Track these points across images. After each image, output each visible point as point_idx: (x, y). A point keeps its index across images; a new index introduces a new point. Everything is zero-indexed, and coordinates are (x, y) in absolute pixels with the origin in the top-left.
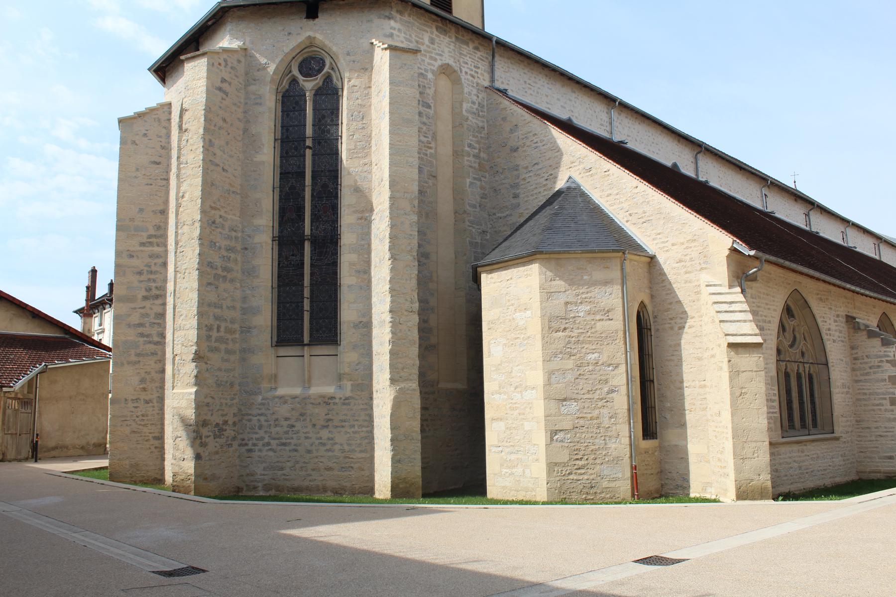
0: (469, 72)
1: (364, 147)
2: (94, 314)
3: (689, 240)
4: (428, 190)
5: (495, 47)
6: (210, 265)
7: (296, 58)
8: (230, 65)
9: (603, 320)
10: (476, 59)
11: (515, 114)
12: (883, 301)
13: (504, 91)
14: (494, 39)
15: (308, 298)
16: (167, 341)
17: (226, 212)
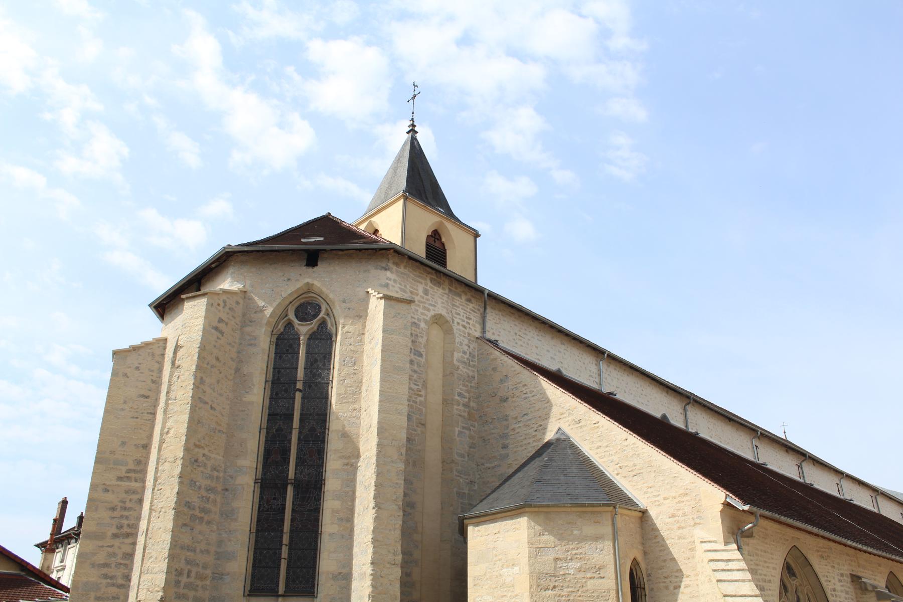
0: (461, 323)
1: (355, 393)
2: (57, 548)
3: (681, 494)
4: (416, 438)
5: (486, 299)
6: (188, 505)
7: (293, 303)
8: (228, 306)
9: (594, 578)
10: (469, 311)
11: (505, 365)
12: (888, 559)
13: (495, 342)
14: (486, 292)
15: (286, 545)
16: (132, 584)
17: (210, 450)
